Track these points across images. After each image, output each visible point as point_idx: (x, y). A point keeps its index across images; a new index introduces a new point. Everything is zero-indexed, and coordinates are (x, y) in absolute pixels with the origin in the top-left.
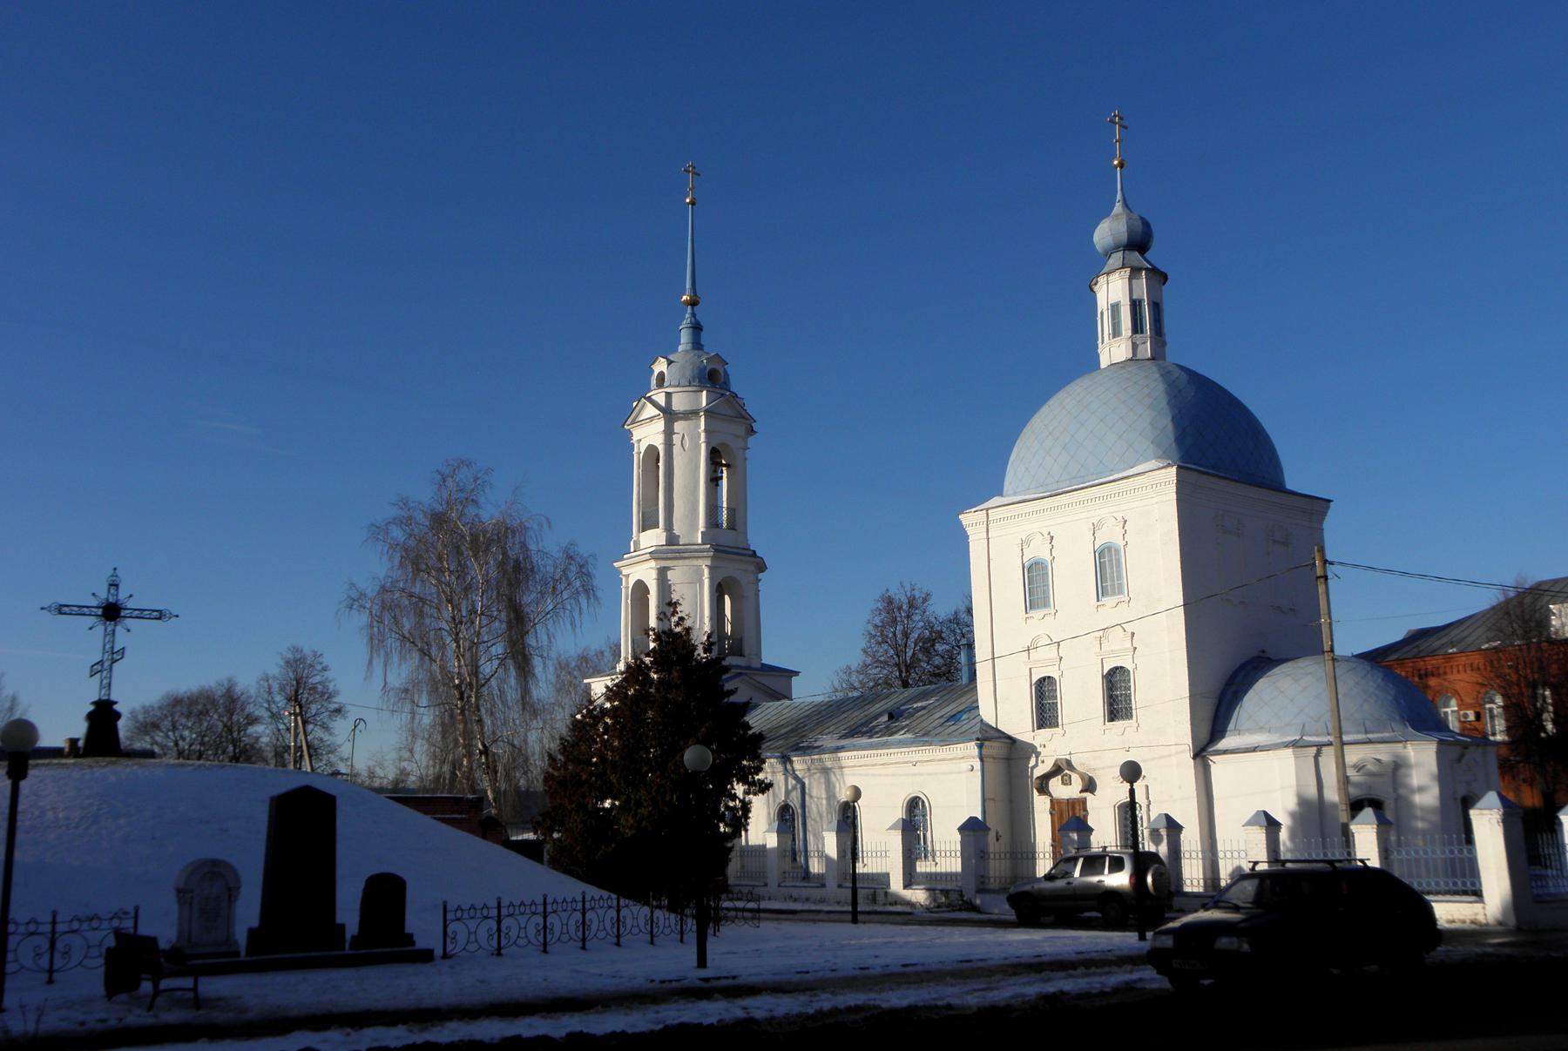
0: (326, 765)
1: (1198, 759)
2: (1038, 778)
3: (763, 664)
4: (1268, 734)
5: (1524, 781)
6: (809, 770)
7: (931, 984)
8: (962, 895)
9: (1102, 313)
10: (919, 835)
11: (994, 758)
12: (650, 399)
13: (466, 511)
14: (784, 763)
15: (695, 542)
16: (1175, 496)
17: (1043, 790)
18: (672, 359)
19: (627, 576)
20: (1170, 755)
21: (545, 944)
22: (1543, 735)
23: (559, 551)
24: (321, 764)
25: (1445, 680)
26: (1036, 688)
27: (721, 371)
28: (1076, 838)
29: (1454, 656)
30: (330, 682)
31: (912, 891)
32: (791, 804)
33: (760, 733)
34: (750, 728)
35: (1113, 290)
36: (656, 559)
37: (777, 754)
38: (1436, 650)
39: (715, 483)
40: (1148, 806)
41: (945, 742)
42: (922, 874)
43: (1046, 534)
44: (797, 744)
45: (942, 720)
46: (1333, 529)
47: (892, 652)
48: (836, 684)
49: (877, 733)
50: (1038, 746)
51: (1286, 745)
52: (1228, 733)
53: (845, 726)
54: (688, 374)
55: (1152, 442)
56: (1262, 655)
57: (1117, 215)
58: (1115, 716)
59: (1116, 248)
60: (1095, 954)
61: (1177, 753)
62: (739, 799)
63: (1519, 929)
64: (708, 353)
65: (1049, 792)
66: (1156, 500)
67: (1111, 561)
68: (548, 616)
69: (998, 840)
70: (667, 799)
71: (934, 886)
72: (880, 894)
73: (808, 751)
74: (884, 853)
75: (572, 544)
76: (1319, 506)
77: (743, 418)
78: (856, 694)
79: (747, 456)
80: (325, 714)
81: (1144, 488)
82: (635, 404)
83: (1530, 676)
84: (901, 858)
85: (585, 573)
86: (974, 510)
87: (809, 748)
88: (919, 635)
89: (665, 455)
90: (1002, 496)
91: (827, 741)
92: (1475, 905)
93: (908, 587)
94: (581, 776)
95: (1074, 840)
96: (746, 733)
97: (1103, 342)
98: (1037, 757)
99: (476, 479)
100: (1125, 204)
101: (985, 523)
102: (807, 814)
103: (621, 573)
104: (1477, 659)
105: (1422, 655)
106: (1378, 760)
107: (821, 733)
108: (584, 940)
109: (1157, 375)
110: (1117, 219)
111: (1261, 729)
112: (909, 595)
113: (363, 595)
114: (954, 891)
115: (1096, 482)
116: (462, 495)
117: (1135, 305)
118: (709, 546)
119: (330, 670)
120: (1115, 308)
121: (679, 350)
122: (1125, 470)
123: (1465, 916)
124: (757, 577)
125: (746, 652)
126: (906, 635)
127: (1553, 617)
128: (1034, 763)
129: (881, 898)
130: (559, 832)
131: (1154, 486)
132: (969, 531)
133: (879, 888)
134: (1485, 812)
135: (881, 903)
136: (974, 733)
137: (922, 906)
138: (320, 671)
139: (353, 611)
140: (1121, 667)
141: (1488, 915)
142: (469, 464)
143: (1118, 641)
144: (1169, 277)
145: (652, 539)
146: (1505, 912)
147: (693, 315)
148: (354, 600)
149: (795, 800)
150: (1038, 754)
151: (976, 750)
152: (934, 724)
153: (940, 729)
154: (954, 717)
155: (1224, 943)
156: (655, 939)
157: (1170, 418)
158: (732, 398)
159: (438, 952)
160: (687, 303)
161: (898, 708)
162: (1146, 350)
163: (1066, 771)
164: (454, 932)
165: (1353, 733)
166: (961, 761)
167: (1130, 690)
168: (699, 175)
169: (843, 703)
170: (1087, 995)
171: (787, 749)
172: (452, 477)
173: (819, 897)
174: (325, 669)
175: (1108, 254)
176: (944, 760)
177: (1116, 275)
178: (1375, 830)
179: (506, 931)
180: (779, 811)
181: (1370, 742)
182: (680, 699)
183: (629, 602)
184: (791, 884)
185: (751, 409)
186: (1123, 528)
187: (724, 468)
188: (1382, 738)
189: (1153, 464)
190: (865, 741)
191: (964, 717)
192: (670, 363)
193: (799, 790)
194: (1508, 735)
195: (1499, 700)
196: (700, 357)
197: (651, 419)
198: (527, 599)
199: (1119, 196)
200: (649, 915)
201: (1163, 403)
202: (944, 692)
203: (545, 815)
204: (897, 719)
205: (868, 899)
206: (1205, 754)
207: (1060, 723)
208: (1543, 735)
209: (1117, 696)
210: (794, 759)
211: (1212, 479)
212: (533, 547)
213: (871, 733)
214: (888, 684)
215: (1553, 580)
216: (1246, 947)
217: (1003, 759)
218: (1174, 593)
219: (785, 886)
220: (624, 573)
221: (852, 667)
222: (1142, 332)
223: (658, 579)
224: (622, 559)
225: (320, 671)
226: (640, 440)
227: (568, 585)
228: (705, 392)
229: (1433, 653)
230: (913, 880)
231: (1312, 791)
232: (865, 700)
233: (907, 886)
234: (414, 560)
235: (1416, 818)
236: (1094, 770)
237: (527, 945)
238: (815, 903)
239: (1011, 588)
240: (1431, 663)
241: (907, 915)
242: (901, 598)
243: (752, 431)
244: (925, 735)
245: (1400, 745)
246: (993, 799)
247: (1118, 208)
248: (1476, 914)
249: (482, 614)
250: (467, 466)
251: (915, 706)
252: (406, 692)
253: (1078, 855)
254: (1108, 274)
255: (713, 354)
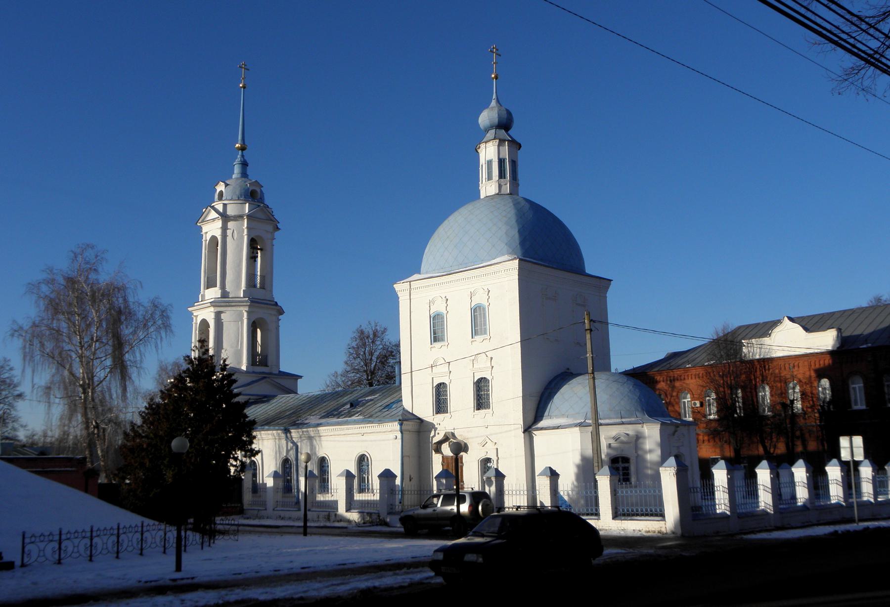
0: (11, 429)
1: (526, 433)
2: (435, 443)
3: (280, 372)
4: (566, 418)
5: (726, 442)
6: (301, 437)
7: (307, 581)
8: (379, 516)
9: (482, 166)
10: (365, 478)
11: (410, 431)
12: (213, 208)
13: (90, 277)
14: (286, 433)
15: (239, 296)
16: (517, 277)
17: (438, 450)
18: (228, 183)
19: (196, 316)
20: (510, 431)
21: (91, 556)
22: (736, 415)
23: (148, 302)
24: (8, 429)
25: (684, 383)
26: (435, 389)
27: (258, 190)
28: (445, 482)
29: (690, 369)
30: (15, 377)
31: (351, 513)
32: (290, 458)
33: (254, 420)
34: (247, 417)
35: (489, 152)
36: (214, 306)
37: (282, 428)
38: (680, 365)
39: (254, 260)
40: (497, 461)
41: (381, 421)
42: (357, 501)
43: (443, 297)
44: (295, 422)
45: (381, 408)
46: (612, 296)
47: (362, 364)
48: (328, 383)
49: (342, 415)
50: (436, 424)
51: (576, 425)
52: (544, 418)
53: (324, 411)
54: (238, 193)
55: (506, 244)
56: (567, 371)
57: (492, 108)
58: (480, 407)
59: (491, 127)
60: (423, 558)
61: (514, 429)
62: (239, 460)
63: (683, 536)
64: (250, 180)
65: (442, 452)
66: (506, 279)
67: (480, 314)
68: (141, 342)
69: (410, 480)
70: (193, 461)
71: (364, 511)
72: (333, 515)
73: (301, 426)
74: (335, 490)
75: (157, 298)
76: (603, 283)
77: (271, 220)
78: (340, 389)
79: (274, 243)
80: (10, 398)
81: (500, 272)
82: (204, 210)
83: (729, 382)
84: (345, 493)
85: (165, 316)
86: (403, 281)
87: (301, 424)
88: (380, 353)
89: (222, 242)
90: (420, 274)
91: (313, 420)
92: (661, 522)
93: (373, 324)
94: (143, 445)
95: (443, 483)
96: (245, 420)
97: (482, 183)
98: (435, 431)
99: (97, 256)
100: (498, 101)
101: (409, 290)
102: (299, 464)
103: (193, 314)
104: (701, 371)
105: (672, 368)
106: (627, 434)
107: (310, 415)
108: (118, 552)
109: (512, 204)
110: (492, 110)
111: (563, 416)
112: (374, 329)
113: (21, 328)
114: (375, 513)
115: (473, 267)
116: (88, 266)
117: (501, 162)
118: (247, 299)
119: (14, 370)
120: (489, 163)
121: (233, 177)
122: (490, 260)
123: (655, 528)
124: (278, 318)
125: (269, 364)
126: (371, 354)
127: (744, 348)
128: (433, 434)
129: (332, 518)
130: (129, 479)
131: (506, 271)
132: (399, 294)
133: (332, 512)
134: (667, 469)
135: (332, 520)
136: (398, 416)
137: (355, 522)
138: (8, 371)
139: (15, 338)
140: (485, 378)
141: (667, 527)
142: (93, 247)
143: (483, 362)
144: (522, 145)
145: (213, 293)
146: (675, 527)
147: (243, 156)
148: (16, 331)
149: (292, 456)
150: (436, 429)
151: (399, 426)
152: (376, 410)
153: (379, 414)
154: (388, 406)
155: (470, 557)
156: (167, 551)
157: (517, 231)
158: (264, 208)
159: (18, 563)
160: (239, 149)
161: (357, 400)
162: (507, 189)
163: (451, 440)
164: (30, 551)
165: (614, 418)
166: (390, 433)
167: (489, 391)
168: (248, 70)
169: (325, 396)
170: (391, 589)
171: (289, 424)
172: (81, 255)
173: (296, 517)
174: (11, 369)
175: (487, 130)
176: (380, 432)
177: (490, 144)
178: (609, 479)
179: (65, 549)
180: (282, 463)
181: (623, 423)
182: (204, 399)
183: (197, 332)
184: (281, 509)
185: (277, 215)
186: (488, 295)
187: (259, 251)
188: (630, 421)
189: (506, 257)
190: (335, 420)
191: (393, 407)
192: (227, 185)
193: (295, 450)
194: (718, 415)
195: (714, 396)
196: (245, 182)
197: (214, 220)
198: (126, 331)
199: (494, 96)
200: (163, 536)
201: (513, 221)
202: (385, 391)
203: (119, 469)
204: (355, 407)
205: (325, 518)
206: (530, 430)
207: (449, 412)
208: (736, 415)
209: (481, 395)
210: (292, 431)
211: (542, 268)
212: (131, 299)
213: (339, 415)
214: (360, 382)
215: (746, 325)
216: (481, 560)
217: (416, 432)
218: (514, 333)
219: (277, 510)
220: (194, 315)
221: (338, 373)
222: (505, 178)
223: (215, 319)
224: (194, 306)
225: (8, 371)
226: (207, 232)
227: (154, 323)
228: (247, 204)
229: (678, 367)
230: (352, 507)
231: (589, 452)
232: (338, 395)
233: (348, 510)
234: (54, 306)
235: (647, 468)
236: (468, 439)
237: (79, 556)
238: (293, 521)
239: (423, 330)
240: (677, 373)
241: (346, 530)
242: (369, 330)
243: (278, 229)
244: (371, 416)
245: (640, 425)
246: (409, 457)
247: (493, 103)
248: (661, 527)
249: (97, 341)
250: (91, 248)
251: (367, 399)
252: (48, 389)
253: (440, 493)
254: (486, 142)
255: (253, 181)
